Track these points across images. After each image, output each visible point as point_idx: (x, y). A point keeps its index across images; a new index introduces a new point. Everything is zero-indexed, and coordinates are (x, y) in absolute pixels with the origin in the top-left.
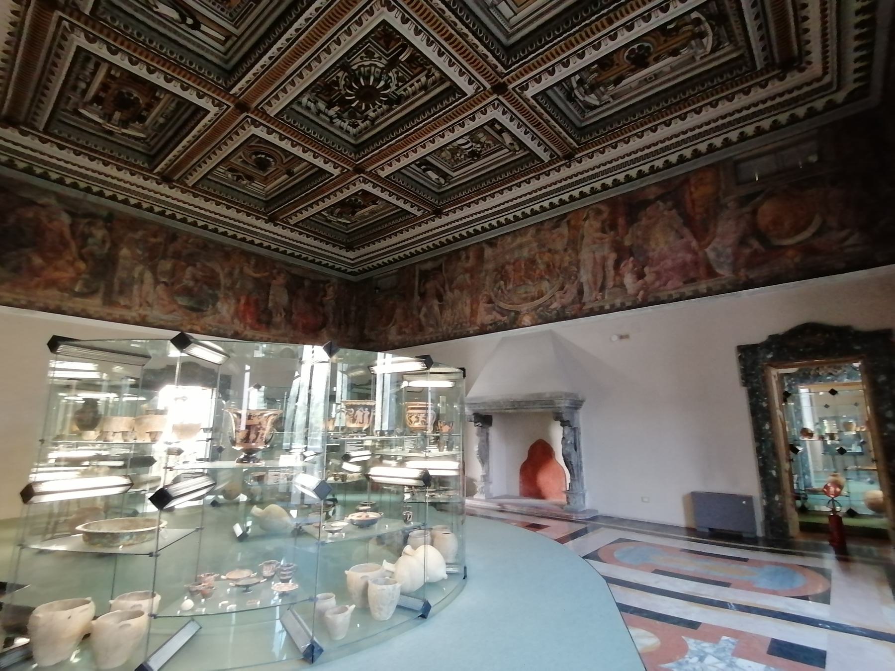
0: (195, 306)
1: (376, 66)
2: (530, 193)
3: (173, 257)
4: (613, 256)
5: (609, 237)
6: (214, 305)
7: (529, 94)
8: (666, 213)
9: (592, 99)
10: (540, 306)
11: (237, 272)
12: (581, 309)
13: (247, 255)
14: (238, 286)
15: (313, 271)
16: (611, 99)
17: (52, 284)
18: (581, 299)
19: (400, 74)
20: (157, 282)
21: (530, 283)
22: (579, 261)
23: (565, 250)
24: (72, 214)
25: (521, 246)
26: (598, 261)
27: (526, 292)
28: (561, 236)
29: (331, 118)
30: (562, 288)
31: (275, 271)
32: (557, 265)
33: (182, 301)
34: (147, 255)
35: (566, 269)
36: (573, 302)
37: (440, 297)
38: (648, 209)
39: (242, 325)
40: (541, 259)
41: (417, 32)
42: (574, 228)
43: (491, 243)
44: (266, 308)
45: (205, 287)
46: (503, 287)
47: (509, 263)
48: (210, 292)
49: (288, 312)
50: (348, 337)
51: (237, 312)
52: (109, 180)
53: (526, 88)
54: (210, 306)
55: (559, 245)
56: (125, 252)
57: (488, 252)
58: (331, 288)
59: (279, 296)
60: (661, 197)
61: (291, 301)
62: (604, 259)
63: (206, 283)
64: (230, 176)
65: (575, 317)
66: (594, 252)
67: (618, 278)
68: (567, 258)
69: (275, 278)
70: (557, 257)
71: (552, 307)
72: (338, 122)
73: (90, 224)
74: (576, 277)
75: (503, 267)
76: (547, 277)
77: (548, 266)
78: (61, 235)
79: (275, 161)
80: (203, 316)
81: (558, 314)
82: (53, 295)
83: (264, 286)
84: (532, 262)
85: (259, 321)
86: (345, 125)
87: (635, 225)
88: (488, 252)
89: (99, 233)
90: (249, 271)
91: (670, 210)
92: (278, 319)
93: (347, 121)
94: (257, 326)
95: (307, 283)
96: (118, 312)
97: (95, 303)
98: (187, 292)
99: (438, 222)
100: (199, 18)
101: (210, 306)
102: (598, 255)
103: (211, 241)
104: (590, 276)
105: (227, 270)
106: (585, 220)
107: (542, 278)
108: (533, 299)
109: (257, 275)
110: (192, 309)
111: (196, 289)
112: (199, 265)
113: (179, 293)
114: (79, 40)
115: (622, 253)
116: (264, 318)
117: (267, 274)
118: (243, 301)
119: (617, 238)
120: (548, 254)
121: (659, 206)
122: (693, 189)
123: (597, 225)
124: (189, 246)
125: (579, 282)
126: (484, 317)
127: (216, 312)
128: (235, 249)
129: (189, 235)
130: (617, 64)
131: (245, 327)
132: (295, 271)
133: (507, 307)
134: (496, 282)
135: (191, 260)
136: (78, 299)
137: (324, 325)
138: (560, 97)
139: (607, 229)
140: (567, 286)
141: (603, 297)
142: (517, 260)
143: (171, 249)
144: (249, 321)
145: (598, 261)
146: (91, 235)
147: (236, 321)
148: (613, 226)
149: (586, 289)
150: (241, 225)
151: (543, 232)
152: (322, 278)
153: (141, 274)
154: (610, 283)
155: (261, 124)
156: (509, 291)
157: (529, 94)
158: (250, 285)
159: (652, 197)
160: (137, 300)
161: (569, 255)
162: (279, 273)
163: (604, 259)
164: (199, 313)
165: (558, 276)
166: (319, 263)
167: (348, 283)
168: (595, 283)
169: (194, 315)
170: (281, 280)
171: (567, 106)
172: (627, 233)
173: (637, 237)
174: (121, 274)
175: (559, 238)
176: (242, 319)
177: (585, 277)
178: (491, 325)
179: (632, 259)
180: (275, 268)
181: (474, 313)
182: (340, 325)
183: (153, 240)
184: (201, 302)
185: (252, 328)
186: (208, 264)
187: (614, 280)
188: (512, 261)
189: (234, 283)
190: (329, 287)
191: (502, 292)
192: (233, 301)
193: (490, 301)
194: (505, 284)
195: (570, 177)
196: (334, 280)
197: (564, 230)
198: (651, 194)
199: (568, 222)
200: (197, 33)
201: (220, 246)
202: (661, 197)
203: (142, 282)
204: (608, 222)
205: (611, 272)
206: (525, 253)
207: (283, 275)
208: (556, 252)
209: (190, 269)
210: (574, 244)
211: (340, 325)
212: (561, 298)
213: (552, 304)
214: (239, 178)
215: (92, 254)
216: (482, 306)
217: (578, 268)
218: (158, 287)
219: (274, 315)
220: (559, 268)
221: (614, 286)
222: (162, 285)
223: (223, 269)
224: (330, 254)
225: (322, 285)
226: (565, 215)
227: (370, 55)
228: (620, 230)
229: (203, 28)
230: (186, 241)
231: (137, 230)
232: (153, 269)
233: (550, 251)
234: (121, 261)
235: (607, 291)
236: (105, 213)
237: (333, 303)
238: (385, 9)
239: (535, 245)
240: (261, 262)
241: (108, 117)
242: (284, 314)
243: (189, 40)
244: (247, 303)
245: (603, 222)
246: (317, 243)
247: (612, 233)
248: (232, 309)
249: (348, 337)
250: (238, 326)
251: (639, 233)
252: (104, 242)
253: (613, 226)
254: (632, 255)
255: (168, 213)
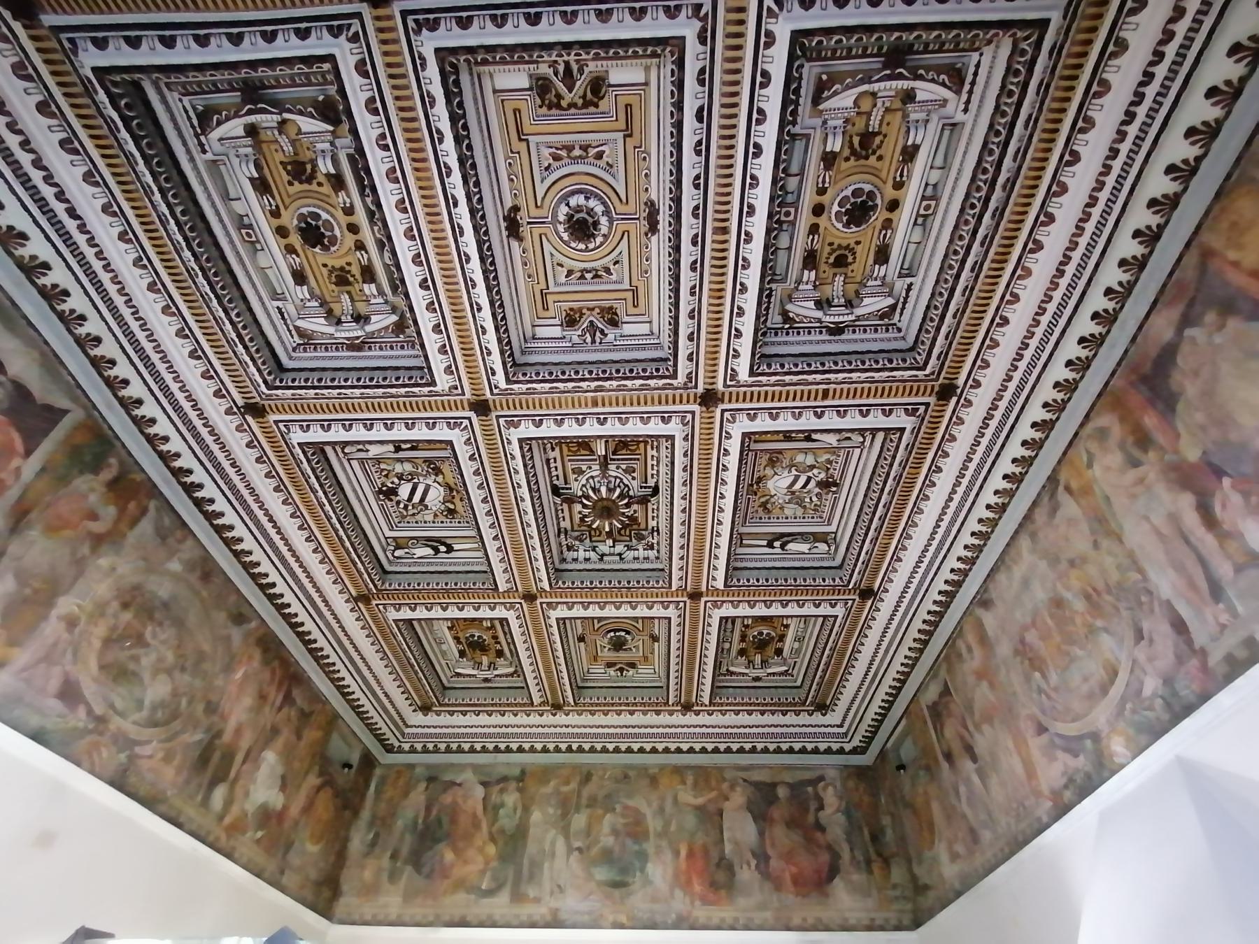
0: (618, 878)
1: (592, 477)
2: (957, 484)
3: (588, 806)
4: (1186, 502)
5: (1151, 466)
6: (642, 870)
7: (743, 375)
8: (1218, 339)
9: (872, 304)
10: (1123, 700)
11: (669, 802)
12: (1204, 668)
13: (678, 770)
14: (673, 828)
15: (789, 768)
16: (908, 280)
17: (460, 885)
18: (1189, 642)
19: (624, 467)
20: (570, 850)
21: (1080, 653)
22: (1131, 555)
23: (1096, 545)
24: (484, 784)
25: (1026, 583)
26: (1166, 530)
27: (1086, 679)
28: (1071, 522)
29: (620, 555)
30: (1139, 636)
31: (725, 786)
32: (1100, 585)
33: (602, 874)
34: (559, 812)
35: (1119, 585)
36: (1180, 660)
37: (970, 750)
38: (1179, 360)
39: (688, 900)
40: (1068, 589)
41: (559, 423)
42: (1083, 493)
43: (983, 600)
44: (722, 858)
45: (629, 842)
46: (1044, 686)
47: (1025, 628)
48: (636, 847)
49: (762, 857)
50: (895, 887)
51: (676, 876)
52: (510, 730)
53: (734, 374)
54: (638, 874)
55: (1080, 543)
56: (536, 816)
57: (989, 619)
58: (830, 790)
59: (740, 829)
60: (1187, 321)
61: (761, 834)
62: (1174, 518)
63: (629, 835)
64: (612, 673)
65: (1205, 697)
66: (1147, 518)
67: (1232, 546)
68: (1109, 561)
69: (727, 799)
70: (1092, 570)
71: (1148, 691)
72: (630, 555)
73: (502, 791)
74: (1150, 593)
75: (1022, 641)
76: (1099, 623)
77: (1088, 597)
78: (475, 816)
79: (628, 633)
80: (630, 894)
81: (1168, 705)
82: (458, 902)
83: (712, 817)
84: (1058, 603)
85: (714, 885)
86: (641, 553)
87: (1180, 407)
88: (989, 619)
89: (511, 798)
90: (688, 797)
91: (1221, 327)
92: (747, 874)
93: (640, 547)
94: (711, 896)
95: (782, 792)
96: (526, 910)
97: (500, 904)
98: (607, 857)
99: (886, 607)
100: (449, 541)
101: (638, 874)
102: (1158, 519)
103: (631, 767)
104: (1171, 573)
105: (655, 804)
106: (1090, 465)
107: (1092, 631)
108: (1105, 689)
109: (700, 801)
110: (617, 885)
111: (617, 849)
112: (618, 808)
113: (594, 863)
114: (392, 615)
115: (1198, 480)
116: (721, 876)
117: (714, 794)
118: (683, 853)
119: (1167, 457)
120: (1074, 573)
121: (1193, 339)
122: (1232, 255)
123: (1115, 459)
124: (606, 783)
125: (1161, 603)
126: (1052, 772)
127: (647, 882)
128: (662, 768)
129: (604, 767)
130: (858, 243)
131: (692, 903)
132: (757, 776)
133: (1071, 729)
134: (1028, 679)
135: (607, 803)
136: (486, 901)
137: (833, 871)
138: (824, 342)
139: (1137, 453)
140: (1146, 626)
141: (1234, 614)
142: (1035, 614)
143: (586, 792)
144: (697, 888)
145: (1166, 530)
146: (502, 805)
147: (679, 893)
148: (1143, 441)
149: (1184, 611)
150: (655, 730)
151: (1041, 535)
152: (808, 775)
153: (553, 844)
154: (1224, 570)
155: (558, 603)
156: (1056, 689)
157: (743, 375)
158: (690, 821)
159: (1168, 335)
160: (547, 885)
161: (1110, 553)
162: (732, 787)
163: (1174, 518)
164: (624, 890)
165: (1117, 609)
166: (791, 751)
167: (861, 773)
168: (1192, 585)
169: (617, 893)
170: (738, 798)
171: (843, 341)
172: (1178, 436)
173: (1203, 428)
174: (531, 848)
175: (1070, 525)
176: (687, 886)
177: (1165, 583)
178: (1066, 787)
179: (1226, 482)
180: (724, 780)
181: (1031, 773)
182: (868, 862)
183: (565, 789)
184: (625, 870)
185: (705, 901)
186: (630, 803)
187: (1229, 557)
188: (1029, 620)
189: (667, 824)
190: (825, 788)
191: (1049, 697)
192: (668, 856)
193: (1042, 730)
194: (1044, 676)
195: (989, 417)
196: (831, 774)
197: (1069, 507)
198: (1163, 327)
199: (1068, 489)
200: (453, 554)
201: (643, 770)
202: (1187, 321)
203: (553, 855)
204: (1130, 440)
205: (1207, 541)
206: (1040, 594)
207: (738, 789)
208: (1084, 560)
209: (609, 817)
210: (1103, 525)
211: (868, 862)
212: (1151, 659)
213: (1142, 683)
214: (621, 670)
215: (502, 831)
216: (1036, 744)
217: (1141, 571)
218: (572, 858)
219: (737, 868)
220: (1109, 592)
221: (1238, 569)
222: (576, 853)
223: (650, 805)
224: (797, 730)
225: (810, 789)
226: (1053, 479)
227: (579, 472)
228: (1160, 438)
229: (456, 547)
230: (602, 778)
231: (549, 781)
232: (566, 832)
233: (1072, 563)
234: (531, 831)
235: (1231, 593)
236: (517, 772)
237: (841, 818)
238: (512, 429)
239: (1043, 565)
240: (703, 776)
241: (478, 665)
242: (753, 863)
243: (455, 564)
244: (691, 854)
245: (1122, 446)
246: (768, 719)
247: (1152, 455)
248: (670, 871)
249: (895, 887)
250: (680, 902)
251: (1199, 417)
252: (515, 810)
253: (1143, 441)
254: (1219, 473)
255: (575, 747)
